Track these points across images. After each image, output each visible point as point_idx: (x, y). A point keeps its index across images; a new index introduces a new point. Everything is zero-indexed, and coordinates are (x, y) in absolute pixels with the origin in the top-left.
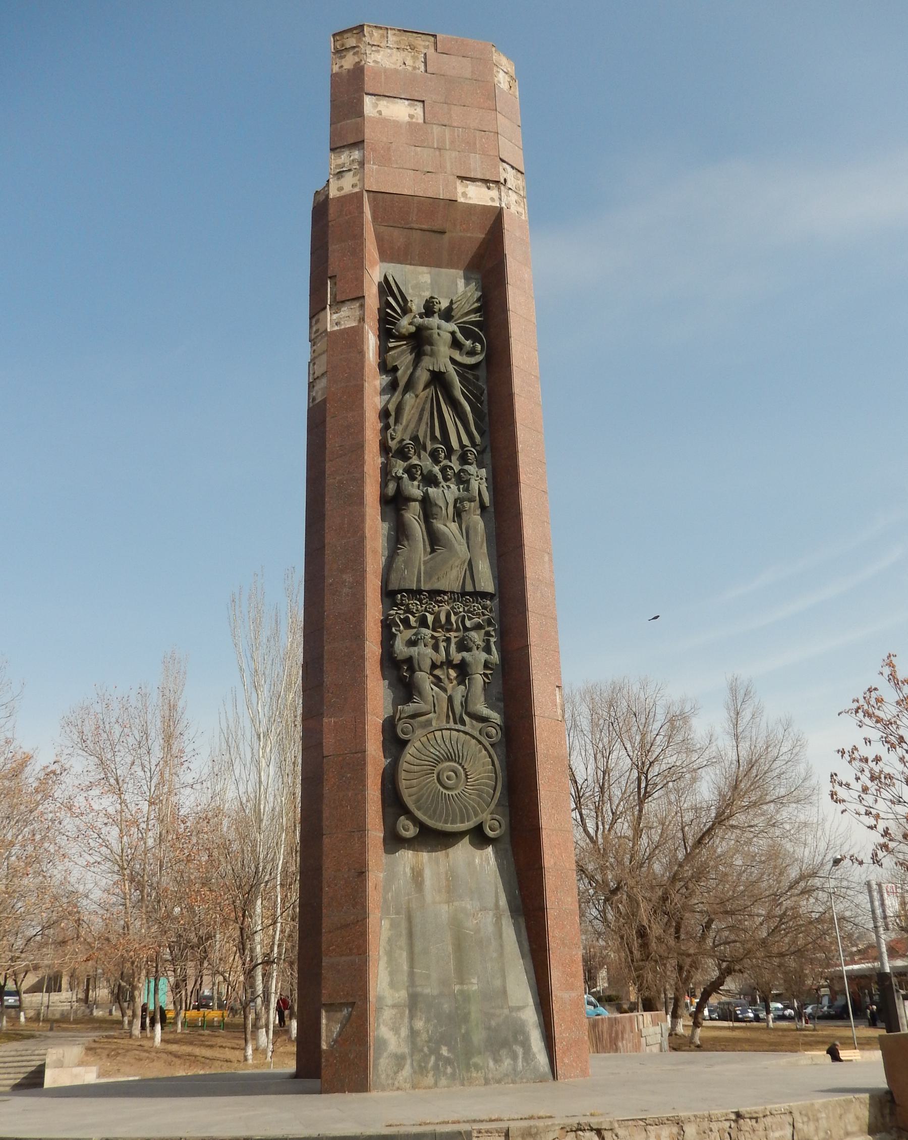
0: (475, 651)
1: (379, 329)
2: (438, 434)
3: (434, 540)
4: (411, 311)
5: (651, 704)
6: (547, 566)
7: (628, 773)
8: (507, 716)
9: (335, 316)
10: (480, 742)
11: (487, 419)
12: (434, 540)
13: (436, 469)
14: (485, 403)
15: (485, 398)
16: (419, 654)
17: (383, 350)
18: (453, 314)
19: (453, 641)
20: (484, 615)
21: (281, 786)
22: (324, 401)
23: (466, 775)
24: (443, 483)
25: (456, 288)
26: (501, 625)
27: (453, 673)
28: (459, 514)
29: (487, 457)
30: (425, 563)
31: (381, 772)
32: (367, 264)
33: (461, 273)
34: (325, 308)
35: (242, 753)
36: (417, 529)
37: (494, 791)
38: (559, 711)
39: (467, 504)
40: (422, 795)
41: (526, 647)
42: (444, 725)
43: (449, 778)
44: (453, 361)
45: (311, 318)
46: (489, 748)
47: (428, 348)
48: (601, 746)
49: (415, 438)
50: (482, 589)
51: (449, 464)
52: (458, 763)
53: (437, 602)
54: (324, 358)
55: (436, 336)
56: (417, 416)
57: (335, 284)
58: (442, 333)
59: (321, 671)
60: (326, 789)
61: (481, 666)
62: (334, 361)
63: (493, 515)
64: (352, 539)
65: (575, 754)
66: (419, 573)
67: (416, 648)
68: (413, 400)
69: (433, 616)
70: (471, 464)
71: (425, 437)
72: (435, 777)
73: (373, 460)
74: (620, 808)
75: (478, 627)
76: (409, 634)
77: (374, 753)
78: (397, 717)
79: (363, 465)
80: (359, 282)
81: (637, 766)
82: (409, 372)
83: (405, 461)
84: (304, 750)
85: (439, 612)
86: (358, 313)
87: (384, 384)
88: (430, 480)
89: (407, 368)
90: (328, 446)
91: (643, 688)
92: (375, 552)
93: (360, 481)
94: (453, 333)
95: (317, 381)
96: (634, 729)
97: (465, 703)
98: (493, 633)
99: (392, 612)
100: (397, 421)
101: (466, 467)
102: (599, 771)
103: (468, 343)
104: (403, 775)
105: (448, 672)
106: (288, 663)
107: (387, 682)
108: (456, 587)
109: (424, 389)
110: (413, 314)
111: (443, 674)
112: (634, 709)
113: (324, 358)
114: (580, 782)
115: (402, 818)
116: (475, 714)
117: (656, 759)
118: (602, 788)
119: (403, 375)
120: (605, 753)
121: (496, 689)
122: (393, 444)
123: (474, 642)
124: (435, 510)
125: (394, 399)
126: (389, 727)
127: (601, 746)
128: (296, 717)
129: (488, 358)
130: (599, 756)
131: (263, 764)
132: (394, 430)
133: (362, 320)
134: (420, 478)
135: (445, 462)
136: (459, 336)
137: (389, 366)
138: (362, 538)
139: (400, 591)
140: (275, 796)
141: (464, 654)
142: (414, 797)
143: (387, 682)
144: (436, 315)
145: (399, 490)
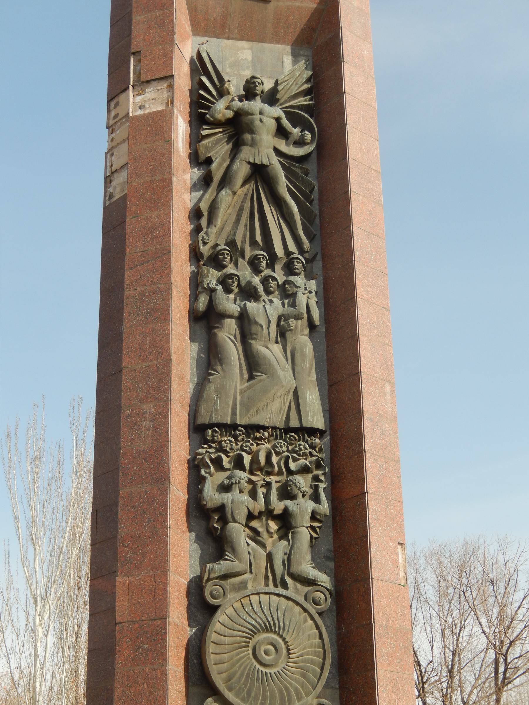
0: (300, 499)
1: (191, 114)
2: (258, 238)
3: (253, 364)
4: (228, 93)
5: (512, 570)
6: (388, 397)
7: (482, 655)
8: (338, 580)
9: (138, 99)
10: (305, 610)
11: (317, 220)
12: (253, 364)
13: (256, 280)
14: (316, 202)
15: (315, 195)
16: (232, 502)
17: (195, 139)
18: (278, 96)
19: (275, 486)
20: (311, 455)
21: (61, 661)
22: (124, 199)
23: (288, 650)
24: (264, 297)
25: (283, 67)
26: (332, 469)
27: (273, 526)
28: (282, 334)
29: (318, 266)
30: (242, 392)
31: (185, 643)
32: (177, 37)
33: (288, 48)
34: (128, 88)
35: (15, 620)
36: (233, 351)
37: (322, 669)
38: (402, 574)
39: (293, 323)
40: (236, 672)
41: (362, 495)
42: (262, 588)
43: (266, 653)
44: (278, 152)
45: (109, 101)
46: (316, 617)
47: (248, 137)
48: (449, 620)
49: (231, 243)
50: (309, 425)
51: (272, 274)
52: (279, 634)
53: (255, 439)
54: (125, 147)
55: (257, 122)
56: (234, 218)
57: (139, 61)
58: (264, 119)
59: (115, 521)
60: (118, 664)
61: (307, 518)
62: (137, 148)
63: (324, 336)
64: (155, 362)
65: (418, 629)
66: (235, 404)
67: (229, 495)
68: (230, 198)
69: (250, 457)
70: (297, 274)
71: (243, 242)
72: (250, 652)
73: (181, 268)
74: (474, 697)
75: (305, 470)
76: (221, 477)
77: (176, 620)
78: (206, 578)
79: (169, 275)
80: (168, 58)
81: (494, 645)
82: (225, 165)
83: (219, 270)
84: (92, 615)
85: (258, 452)
86: (165, 94)
87: (196, 178)
88: (249, 293)
89: (224, 160)
90: (127, 251)
91: (503, 550)
92: (182, 377)
93: (165, 293)
94: (278, 120)
95: (116, 175)
96: (491, 600)
97: (288, 563)
98: (322, 478)
99: (201, 451)
100: (210, 223)
101: (292, 278)
102: (448, 651)
103: (296, 131)
104: (211, 648)
105: (267, 524)
106: (72, 512)
107: (193, 535)
108: (279, 422)
109: (243, 185)
110: (230, 97)
111: (262, 526)
112: (491, 576)
113: (125, 147)
114: (424, 663)
115: (210, 700)
116: (299, 576)
117: (518, 638)
118: (451, 672)
119: (217, 169)
120: (453, 629)
121: (326, 545)
122: (205, 250)
123: (300, 489)
124: (254, 329)
125: (207, 196)
126: (196, 589)
127: (449, 620)
128: (80, 577)
129: (319, 147)
130: (448, 632)
131: (40, 633)
132: (206, 233)
133: (170, 102)
134: (236, 290)
135: (268, 272)
136: (286, 123)
137: (202, 158)
138: (167, 362)
139: (211, 426)
140: (53, 673)
141: (288, 502)
142: (224, 675)
143: (193, 535)
144: (258, 98)
145: (211, 304)
